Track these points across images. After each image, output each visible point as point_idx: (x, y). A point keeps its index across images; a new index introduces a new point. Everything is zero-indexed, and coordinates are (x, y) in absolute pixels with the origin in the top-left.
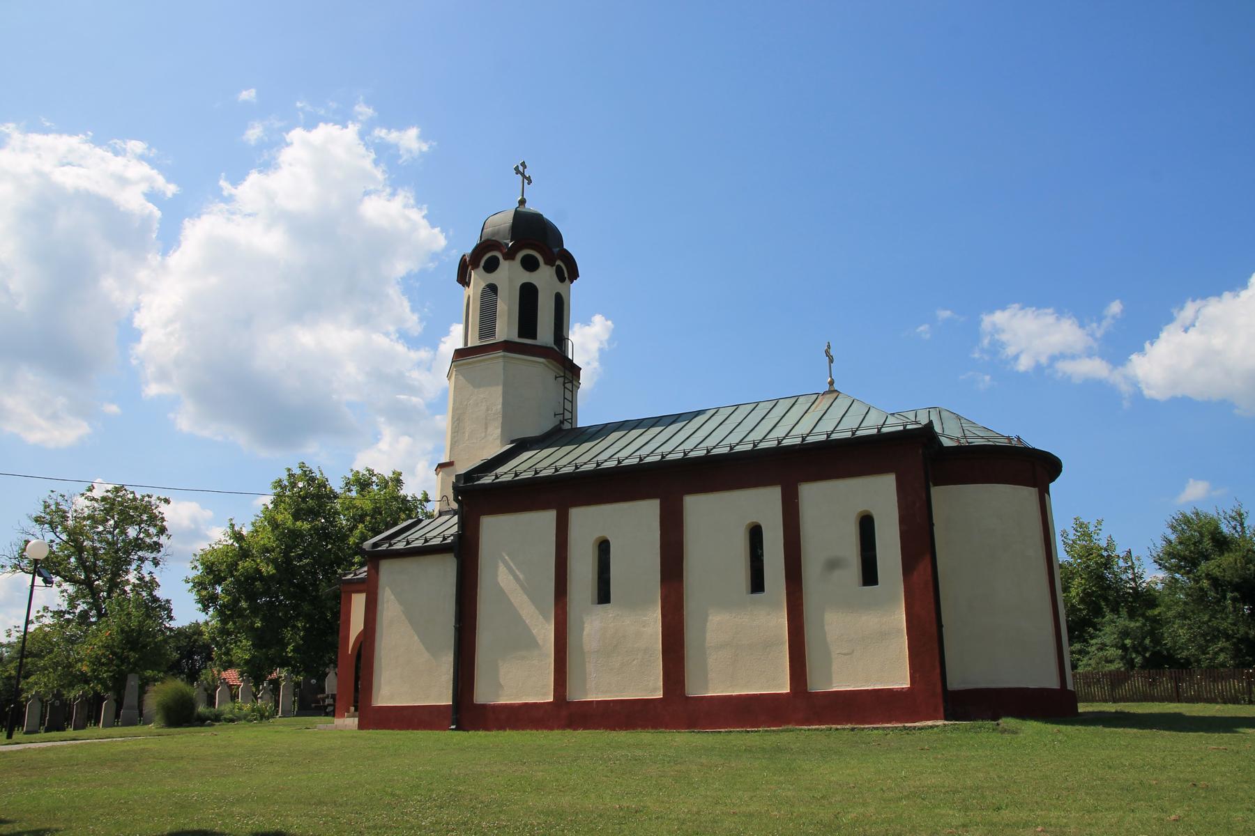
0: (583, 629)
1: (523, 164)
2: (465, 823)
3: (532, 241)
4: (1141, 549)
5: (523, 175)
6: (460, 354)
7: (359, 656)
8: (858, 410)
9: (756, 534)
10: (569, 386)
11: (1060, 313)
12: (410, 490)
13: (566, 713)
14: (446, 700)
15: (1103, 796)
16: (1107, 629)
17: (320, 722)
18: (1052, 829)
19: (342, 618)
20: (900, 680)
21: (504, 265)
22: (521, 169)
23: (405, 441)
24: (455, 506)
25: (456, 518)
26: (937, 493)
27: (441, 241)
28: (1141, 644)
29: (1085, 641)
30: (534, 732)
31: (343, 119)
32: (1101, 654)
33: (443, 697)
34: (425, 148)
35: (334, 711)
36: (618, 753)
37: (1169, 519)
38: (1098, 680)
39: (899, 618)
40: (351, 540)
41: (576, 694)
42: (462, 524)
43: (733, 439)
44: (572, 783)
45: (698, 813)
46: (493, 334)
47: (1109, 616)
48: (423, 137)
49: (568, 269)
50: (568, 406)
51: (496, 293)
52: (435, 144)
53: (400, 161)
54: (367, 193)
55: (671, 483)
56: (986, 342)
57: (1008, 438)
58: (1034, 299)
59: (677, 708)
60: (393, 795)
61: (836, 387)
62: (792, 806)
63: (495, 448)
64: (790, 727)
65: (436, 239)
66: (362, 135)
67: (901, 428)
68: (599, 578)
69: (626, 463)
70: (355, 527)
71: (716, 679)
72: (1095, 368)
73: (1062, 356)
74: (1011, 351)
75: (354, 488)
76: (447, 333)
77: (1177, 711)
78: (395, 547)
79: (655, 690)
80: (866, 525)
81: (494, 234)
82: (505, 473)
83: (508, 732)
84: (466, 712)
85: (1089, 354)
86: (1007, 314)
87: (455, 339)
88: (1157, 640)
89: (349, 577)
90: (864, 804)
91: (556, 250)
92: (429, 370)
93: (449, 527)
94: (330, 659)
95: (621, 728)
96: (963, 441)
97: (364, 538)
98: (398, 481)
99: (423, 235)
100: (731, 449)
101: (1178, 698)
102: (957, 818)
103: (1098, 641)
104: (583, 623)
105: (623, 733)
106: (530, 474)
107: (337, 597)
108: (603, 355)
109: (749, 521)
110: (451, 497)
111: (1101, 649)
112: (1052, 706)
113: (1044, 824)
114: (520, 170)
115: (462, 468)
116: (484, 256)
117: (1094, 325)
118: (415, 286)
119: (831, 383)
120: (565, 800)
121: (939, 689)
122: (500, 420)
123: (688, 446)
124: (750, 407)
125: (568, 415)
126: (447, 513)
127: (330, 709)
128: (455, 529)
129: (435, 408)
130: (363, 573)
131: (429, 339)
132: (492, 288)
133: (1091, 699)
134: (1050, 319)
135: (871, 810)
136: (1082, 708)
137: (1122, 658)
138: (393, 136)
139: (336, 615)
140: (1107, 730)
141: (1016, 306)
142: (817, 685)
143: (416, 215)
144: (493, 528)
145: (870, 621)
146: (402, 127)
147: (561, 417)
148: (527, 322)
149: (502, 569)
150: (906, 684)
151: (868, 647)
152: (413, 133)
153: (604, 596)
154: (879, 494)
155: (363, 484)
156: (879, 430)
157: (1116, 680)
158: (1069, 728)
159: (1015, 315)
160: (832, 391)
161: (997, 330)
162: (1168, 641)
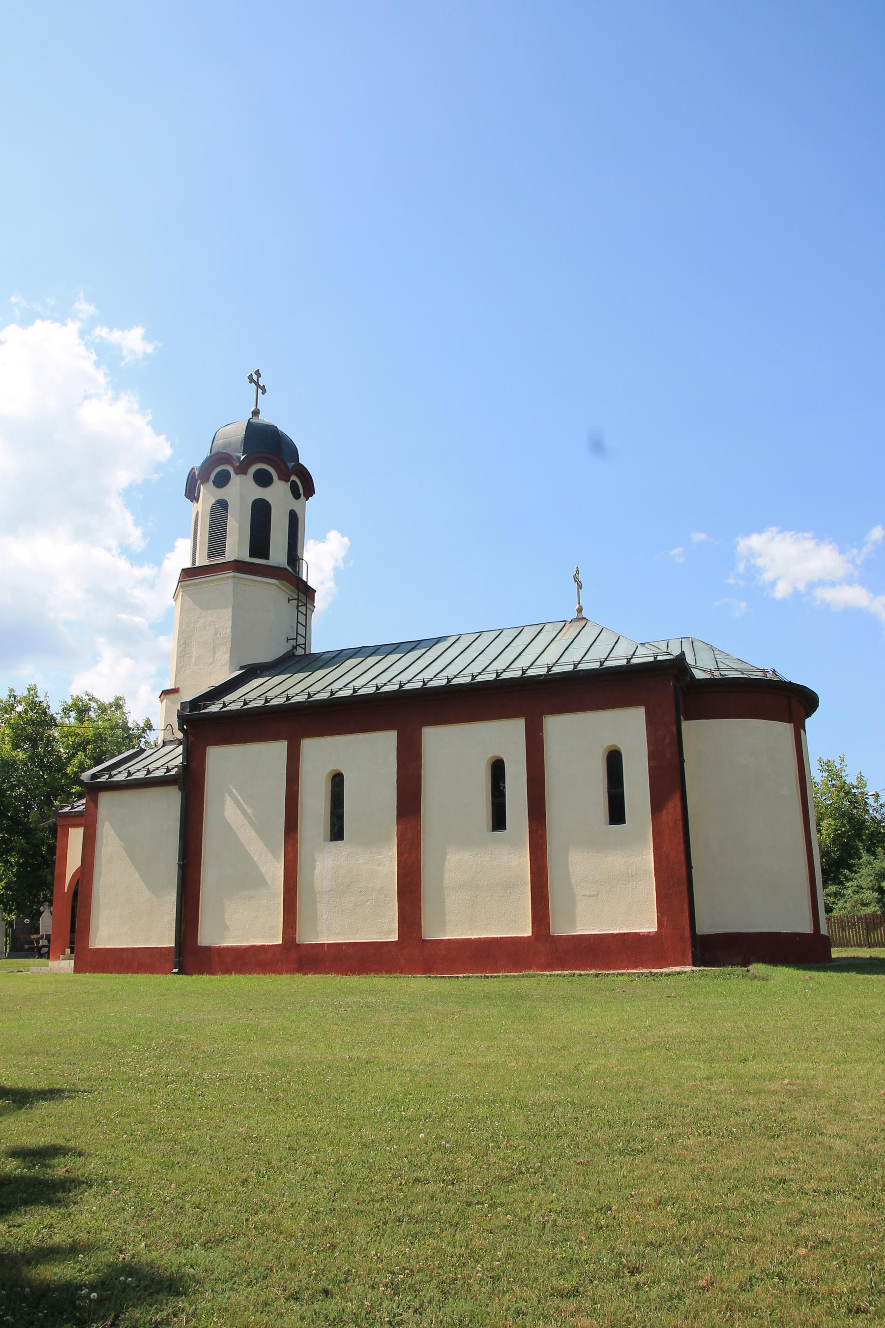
0: (314, 868)
1: (258, 373)
2: (186, 1075)
3: (268, 452)
5: (257, 384)
6: (188, 574)
7: (75, 894)
8: (606, 641)
9: (498, 769)
10: (302, 609)
11: (820, 538)
12: (135, 717)
13: (295, 956)
14: (169, 942)
15: (853, 1046)
16: (863, 871)
17: (34, 965)
18: (798, 1082)
19: (58, 851)
20: (645, 921)
21: (236, 480)
22: (255, 377)
23: (126, 663)
24: (180, 735)
25: (180, 749)
26: (688, 727)
27: (165, 451)
29: (841, 883)
30: (261, 976)
31: (61, 316)
32: (856, 897)
33: (164, 937)
34: (150, 349)
35: (48, 953)
36: (349, 999)
38: (854, 924)
39: (647, 858)
40: (69, 770)
41: (306, 937)
43: (475, 668)
44: (300, 1031)
45: (432, 1064)
46: (222, 553)
48: (148, 338)
49: (303, 485)
50: (301, 630)
51: (227, 511)
52: (160, 345)
53: (122, 364)
54: (86, 397)
56: (741, 567)
57: (763, 671)
58: (790, 523)
59: (413, 951)
60: (110, 1044)
61: (584, 614)
62: (531, 1057)
64: (531, 972)
65: (160, 448)
66: (83, 334)
67: (652, 659)
68: (332, 814)
69: (361, 692)
70: (74, 755)
71: (454, 920)
72: (854, 596)
73: (821, 583)
74: (768, 576)
75: (73, 714)
76: (172, 549)
78: (115, 779)
79: (390, 932)
80: (614, 760)
81: (225, 446)
82: (233, 701)
83: (234, 976)
84: (189, 954)
85: (849, 581)
86: (764, 537)
87: (182, 555)
89: (66, 810)
90: (607, 1055)
91: (291, 465)
92: (152, 588)
93: (173, 758)
94: (45, 897)
95: (353, 973)
96: (716, 673)
97: (83, 769)
98: (118, 705)
99: (148, 445)
100: (473, 678)
102: (701, 1069)
103: (855, 883)
104: (315, 861)
105: (356, 978)
106: (260, 703)
107: (53, 830)
108: (339, 574)
109: (490, 755)
110: (176, 726)
111: (856, 892)
112: (804, 951)
113: (791, 1076)
114: (254, 379)
115: (188, 696)
116: (215, 470)
117: (855, 551)
118: (138, 498)
119: (580, 610)
120: (292, 1050)
121: (687, 933)
122: (229, 644)
123: (427, 675)
124: (494, 635)
125: (301, 640)
126: (171, 742)
127: (44, 950)
128: (180, 760)
129: (159, 628)
130: (81, 805)
131: (153, 554)
132: (222, 505)
133: (846, 944)
134: (810, 545)
135: (614, 1061)
136: (836, 953)
137: (879, 901)
138: (116, 336)
139: (52, 849)
140: (861, 976)
141: (774, 529)
142: (560, 928)
143: (140, 422)
144: (222, 760)
146: (125, 325)
147: (293, 643)
148: (259, 542)
149: (229, 804)
150: (654, 929)
151: (613, 887)
152: (137, 333)
153: (337, 833)
154: (627, 727)
155: (81, 710)
156: (629, 661)
157: (871, 924)
158: (822, 974)
159: (773, 538)
161: (753, 553)
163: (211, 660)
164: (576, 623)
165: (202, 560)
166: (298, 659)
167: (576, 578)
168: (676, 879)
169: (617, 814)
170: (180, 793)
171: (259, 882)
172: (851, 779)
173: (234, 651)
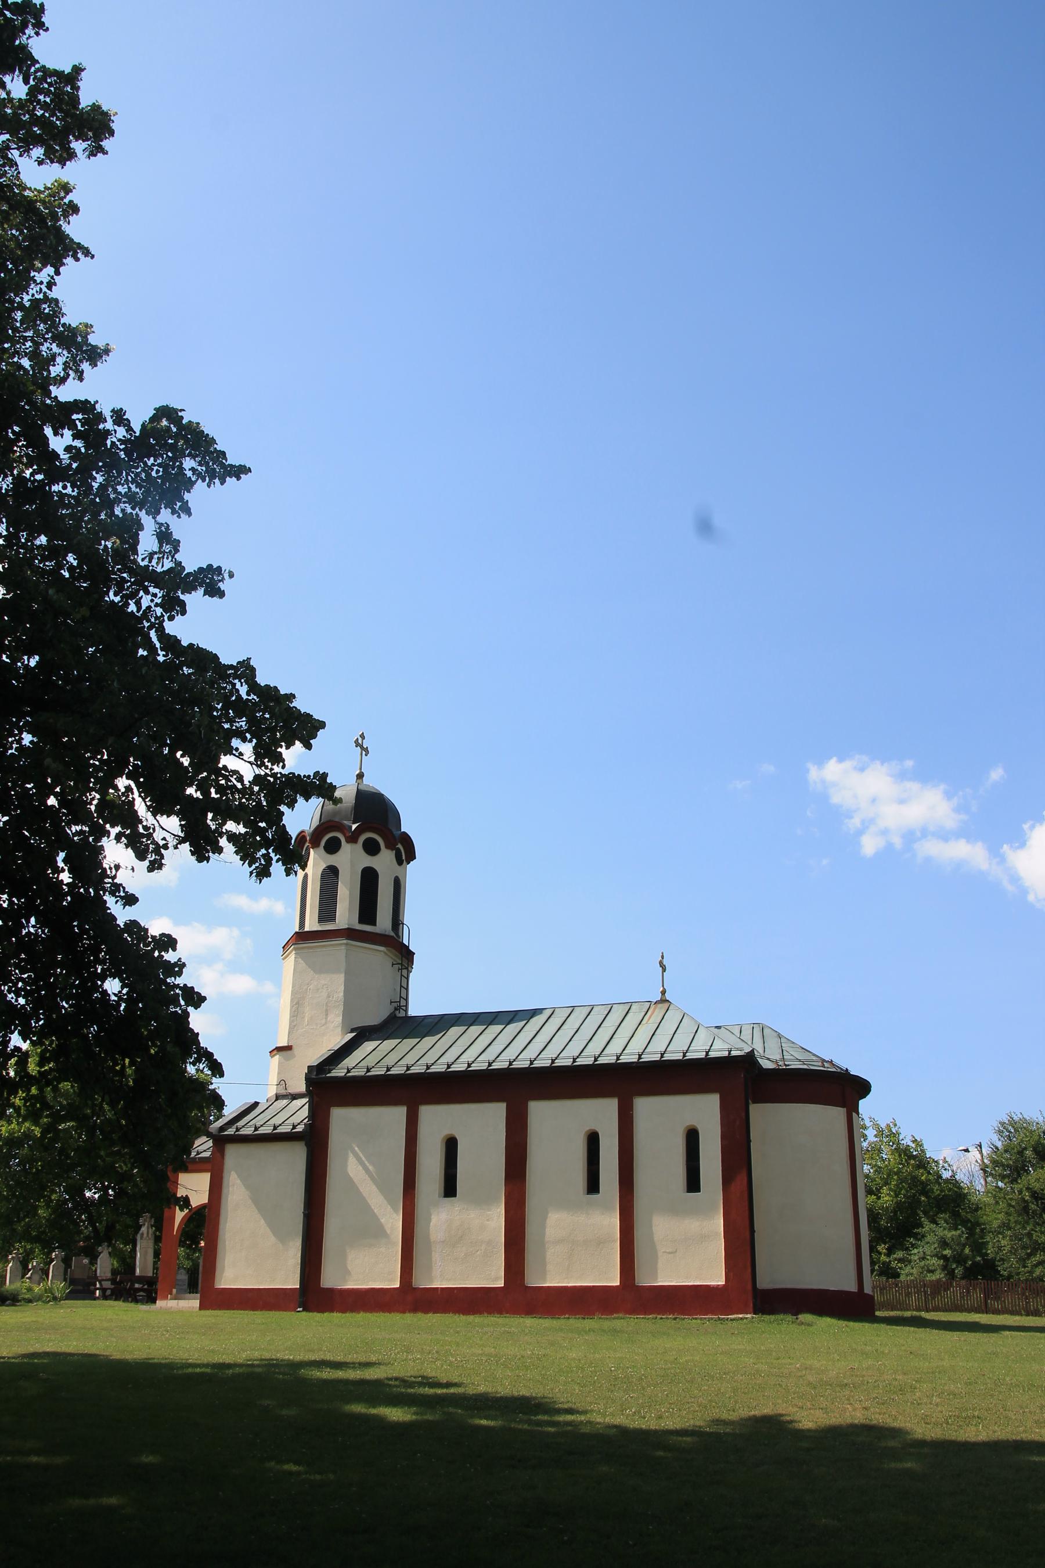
0: (430, 1220)
1: (362, 736)
4: (961, 1152)
5: (362, 747)
6: (302, 937)
8: (688, 1027)
9: (593, 1140)
10: (405, 972)
14: (293, 1282)
16: (929, 1238)
20: (717, 1277)
21: (346, 848)
28: (961, 1254)
29: (907, 1249)
33: (290, 1280)
37: (996, 1124)
39: (718, 1223)
42: (313, 1114)
47: (928, 1226)
49: (405, 850)
50: (404, 995)
55: (516, 1088)
61: (668, 996)
63: (337, 1039)
64: (621, 1315)
67: (726, 1054)
73: (925, 833)
77: (977, 1320)
79: (497, 1279)
80: (692, 1137)
84: (313, 1294)
85: (964, 833)
88: (979, 1247)
96: (780, 1063)
101: (986, 1310)
111: (924, 1258)
119: (663, 992)
121: (749, 1287)
122: (342, 1008)
124: (587, 1010)
125: (403, 1003)
136: (878, 1313)
137: (944, 1268)
142: (644, 1280)
144: (344, 1120)
145: (692, 1225)
147: (395, 1005)
148: (367, 910)
150: (721, 1282)
151: (690, 1250)
153: (450, 1189)
154: (705, 1111)
157: (937, 1288)
160: (663, 1001)
162: (990, 1251)
163: (323, 1021)
164: (660, 1005)
165: (312, 924)
166: (399, 1024)
167: (661, 964)
168: (741, 1242)
169: (693, 1184)
170: (305, 1149)
171: (379, 1232)
172: (907, 1141)
173: (346, 1014)
